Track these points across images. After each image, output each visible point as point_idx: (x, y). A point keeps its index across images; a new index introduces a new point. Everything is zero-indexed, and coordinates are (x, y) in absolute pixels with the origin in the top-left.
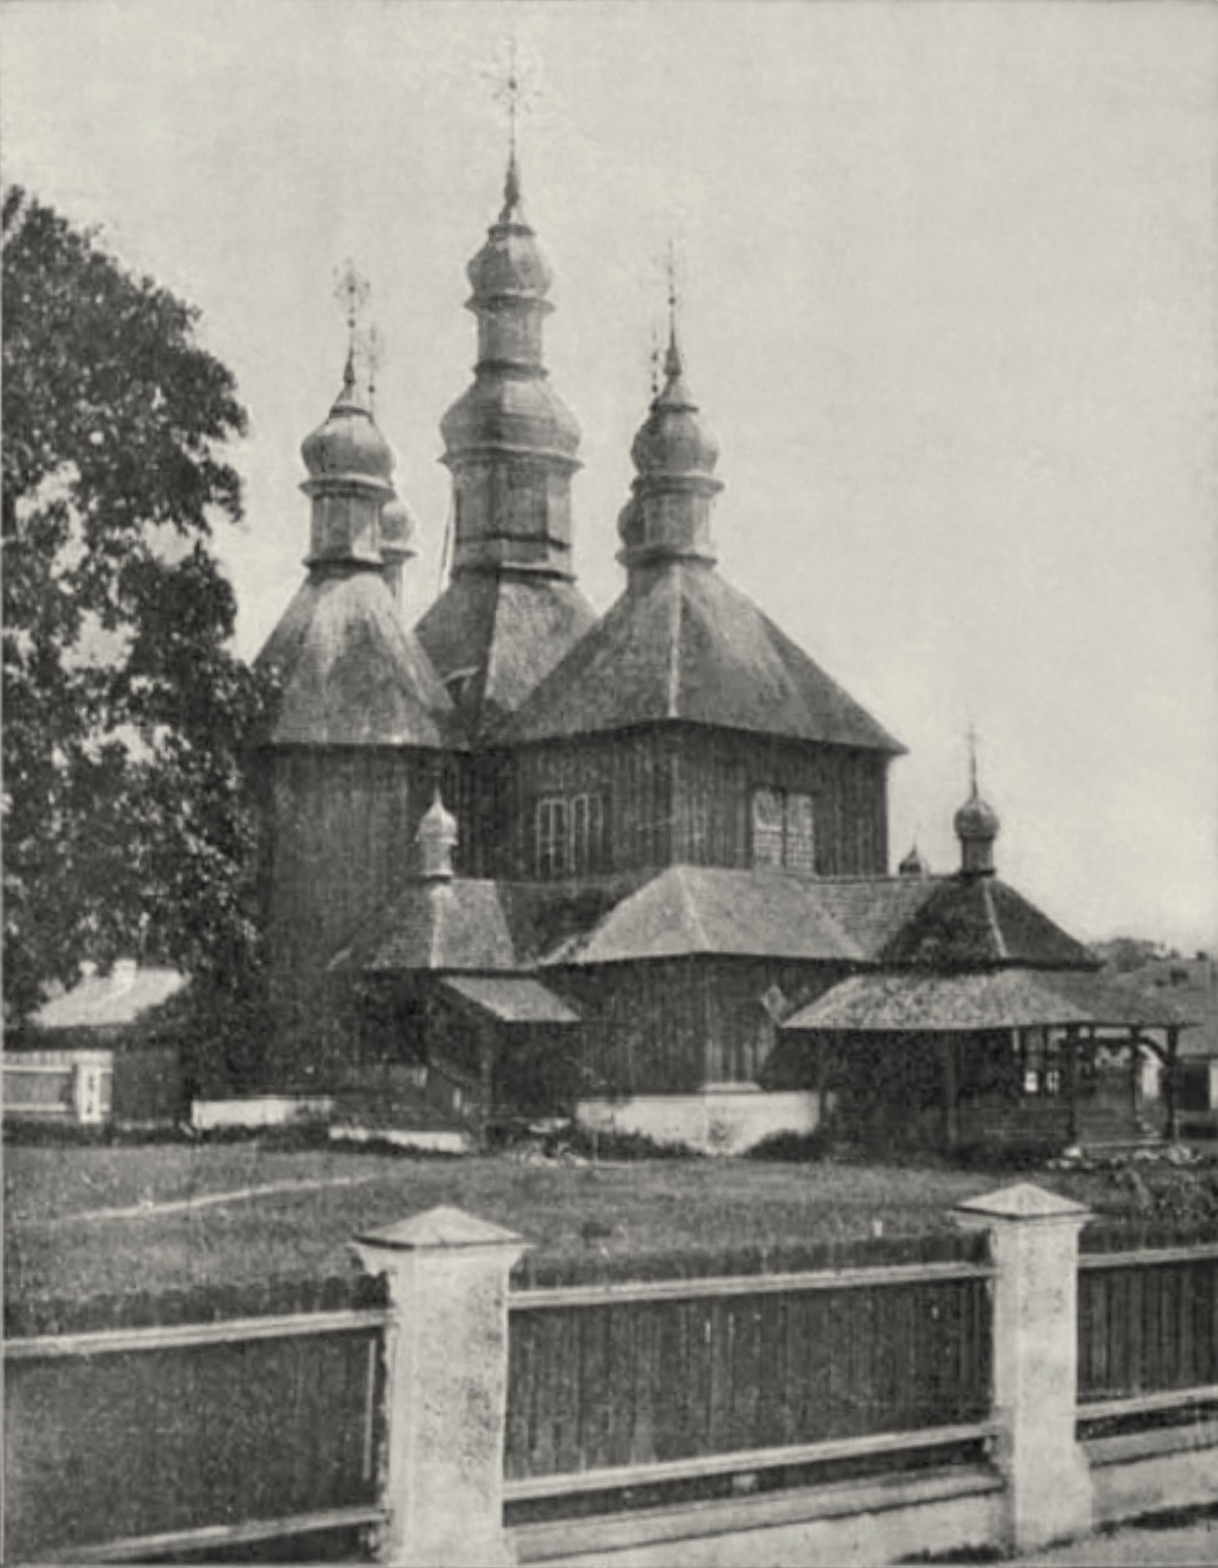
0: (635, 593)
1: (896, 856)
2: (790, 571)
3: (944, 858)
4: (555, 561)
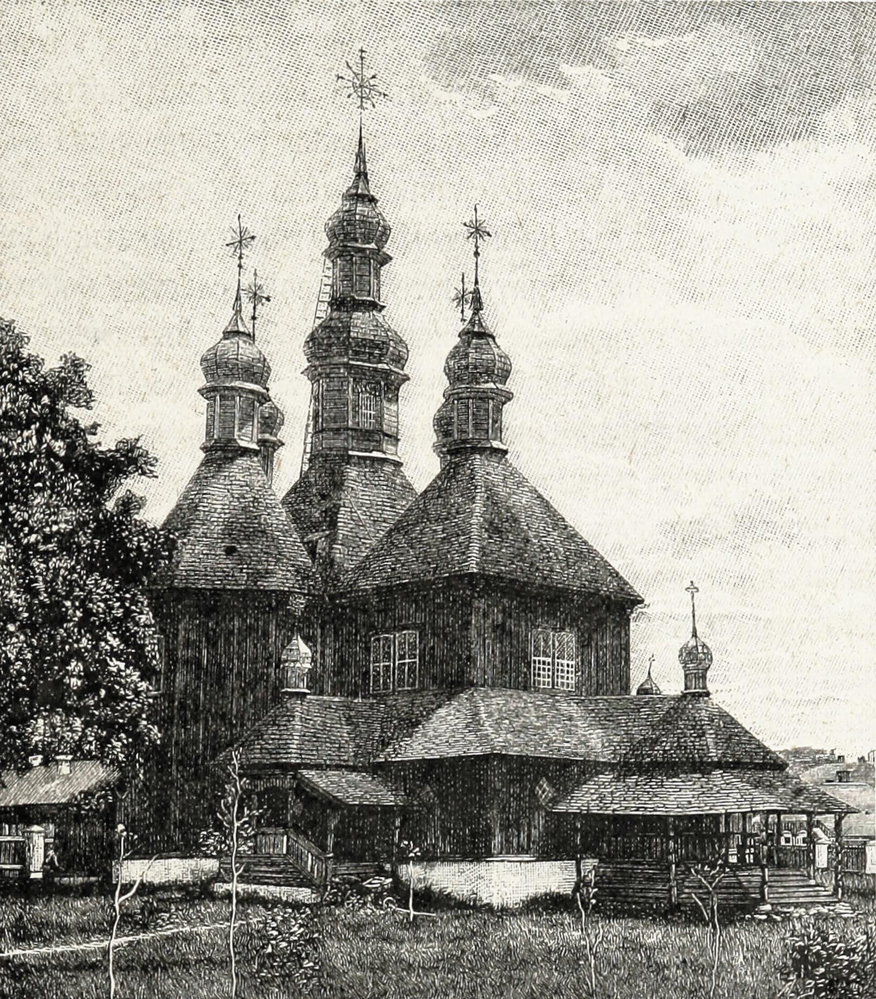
0: (449, 473)
1: (637, 679)
2: (580, 469)
3: (672, 684)
4: (389, 451)
